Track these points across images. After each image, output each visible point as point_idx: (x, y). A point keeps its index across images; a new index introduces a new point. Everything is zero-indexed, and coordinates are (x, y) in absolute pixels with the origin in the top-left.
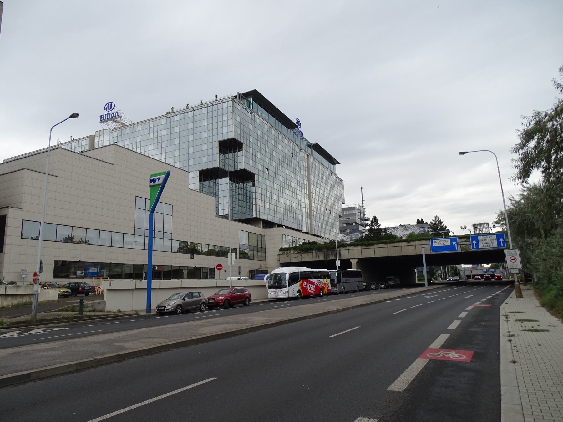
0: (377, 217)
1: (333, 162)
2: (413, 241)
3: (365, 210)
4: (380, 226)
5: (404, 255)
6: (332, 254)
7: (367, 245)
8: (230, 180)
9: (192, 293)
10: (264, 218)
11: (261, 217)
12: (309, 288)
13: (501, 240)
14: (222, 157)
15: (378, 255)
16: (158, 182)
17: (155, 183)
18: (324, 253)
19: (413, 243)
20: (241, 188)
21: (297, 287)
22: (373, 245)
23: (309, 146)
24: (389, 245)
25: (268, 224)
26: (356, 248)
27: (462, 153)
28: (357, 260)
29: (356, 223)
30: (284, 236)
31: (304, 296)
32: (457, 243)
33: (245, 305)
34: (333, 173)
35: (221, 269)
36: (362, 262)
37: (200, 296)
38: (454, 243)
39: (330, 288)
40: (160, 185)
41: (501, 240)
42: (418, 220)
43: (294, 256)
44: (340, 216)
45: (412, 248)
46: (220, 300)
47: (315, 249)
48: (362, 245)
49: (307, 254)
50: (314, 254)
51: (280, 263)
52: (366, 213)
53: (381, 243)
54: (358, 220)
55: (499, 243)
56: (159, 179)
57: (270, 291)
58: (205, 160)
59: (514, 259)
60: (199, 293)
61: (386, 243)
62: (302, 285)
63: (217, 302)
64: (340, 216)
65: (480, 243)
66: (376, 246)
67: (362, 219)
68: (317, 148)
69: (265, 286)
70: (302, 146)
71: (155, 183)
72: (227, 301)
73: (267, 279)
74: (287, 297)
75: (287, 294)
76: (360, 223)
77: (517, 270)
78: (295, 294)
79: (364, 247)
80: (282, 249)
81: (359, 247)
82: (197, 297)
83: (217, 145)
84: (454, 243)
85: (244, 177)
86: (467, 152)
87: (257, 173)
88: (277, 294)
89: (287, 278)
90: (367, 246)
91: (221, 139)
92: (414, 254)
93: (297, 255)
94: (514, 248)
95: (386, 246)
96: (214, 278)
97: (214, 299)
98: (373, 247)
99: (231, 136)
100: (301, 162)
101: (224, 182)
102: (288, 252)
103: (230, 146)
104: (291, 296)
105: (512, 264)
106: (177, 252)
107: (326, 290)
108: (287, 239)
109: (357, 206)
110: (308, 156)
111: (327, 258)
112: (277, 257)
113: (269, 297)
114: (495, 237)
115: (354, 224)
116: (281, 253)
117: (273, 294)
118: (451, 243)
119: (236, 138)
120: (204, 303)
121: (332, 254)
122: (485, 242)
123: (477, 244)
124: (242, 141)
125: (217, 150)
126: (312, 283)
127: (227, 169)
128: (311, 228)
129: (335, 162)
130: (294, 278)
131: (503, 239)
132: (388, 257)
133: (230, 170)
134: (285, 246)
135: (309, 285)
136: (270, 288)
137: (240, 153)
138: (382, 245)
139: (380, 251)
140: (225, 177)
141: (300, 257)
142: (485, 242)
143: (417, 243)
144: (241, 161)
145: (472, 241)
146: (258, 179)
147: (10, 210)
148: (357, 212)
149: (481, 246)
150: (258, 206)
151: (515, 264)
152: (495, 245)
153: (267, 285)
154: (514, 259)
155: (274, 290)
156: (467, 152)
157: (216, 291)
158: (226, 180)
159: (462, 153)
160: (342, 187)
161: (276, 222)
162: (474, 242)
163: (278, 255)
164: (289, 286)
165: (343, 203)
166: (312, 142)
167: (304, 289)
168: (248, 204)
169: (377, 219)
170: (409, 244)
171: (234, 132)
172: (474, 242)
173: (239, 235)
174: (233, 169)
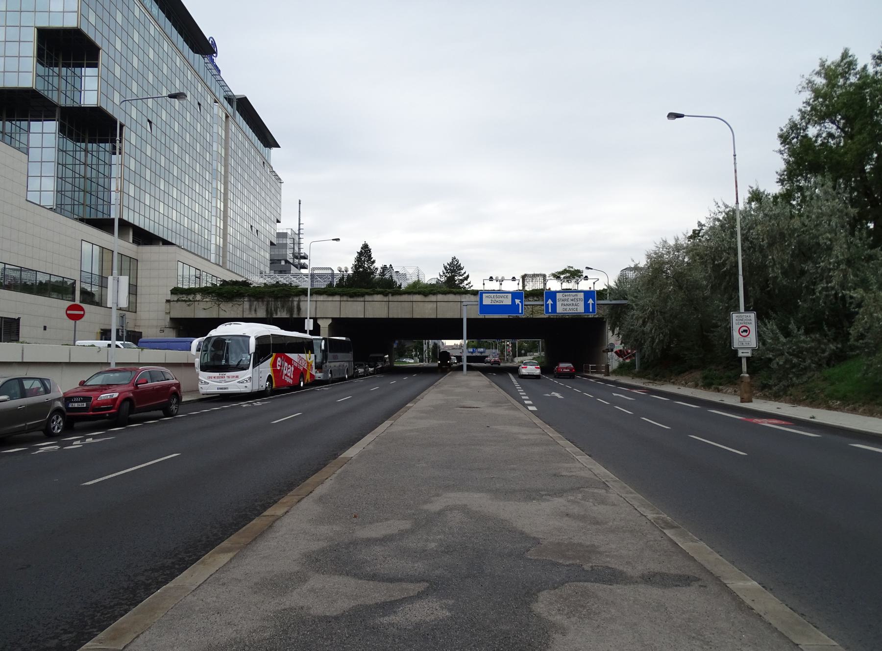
0: (370, 246)
1: (268, 141)
2: (434, 294)
3: (302, 241)
4: (374, 262)
5: (416, 316)
6: (283, 307)
7: (352, 295)
8: (62, 129)
9: (20, 380)
10: (136, 224)
11: (131, 221)
12: (285, 372)
13: (591, 301)
14: (42, 70)
15: (370, 315)
18: (267, 305)
19: (432, 298)
20: (86, 151)
21: (266, 368)
22: (363, 295)
23: (230, 99)
24: (391, 298)
25: (144, 237)
26: (330, 298)
27: (673, 116)
28: (330, 321)
29: (287, 261)
30: (180, 264)
31: (277, 389)
32: (521, 302)
33: (168, 413)
34: (265, 163)
35: (79, 317)
36: (338, 325)
37: (47, 391)
38: (517, 301)
39: (313, 373)
43: (202, 305)
44: (272, 244)
45: (430, 305)
46: (105, 402)
47: (249, 296)
48: (342, 295)
49: (231, 305)
50: (246, 305)
51: (173, 320)
52: (302, 246)
53: (378, 293)
54: (290, 257)
55: (586, 306)
57: (204, 376)
59: (745, 331)
60: (42, 380)
61: (386, 295)
62: (274, 365)
63: (98, 407)
64: (272, 244)
65: (559, 304)
66: (367, 298)
67: (295, 257)
68: (244, 107)
69: (192, 365)
70: (217, 94)
72: (128, 404)
73: (198, 350)
74: (248, 390)
75: (249, 384)
76: (291, 261)
77: (749, 351)
78: (264, 384)
79: (345, 298)
80: (175, 291)
81: (337, 298)
82: (35, 392)
83: (31, 36)
84: (517, 301)
85: (92, 127)
86: (681, 116)
87: (128, 124)
88: (223, 385)
89: (252, 349)
90: (351, 296)
91: (44, 24)
92: (434, 316)
93: (209, 305)
94: (747, 309)
95: (386, 299)
96: (17, 340)
97: (86, 399)
98: (362, 299)
99: (71, 22)
100: (215, 126)
101: (44, 134)
102: (191, 297)
103: (65, 48)
104: (256, 388)
105: (742, 339)
106: (54, 210)
107: (308, 377)
108: (186, 273)
109: (289, 232)
110: (227, 117)
111: (272, 314)
112: (164, 306)
113: (202, 391)
114: (582, 295)
115: (283, 263)
116: (175, 298)
117: (212, 383)
119: (85, 29)
120: (58, 411)
121: (283, 307)
122: (566, 303)
123: (554, 306)
124: (98, 42)
125: (30, 48)
126: (290, 361)
127: (55, 99)
128: (224, 257)
129: (271, 141)
130: (265, 348)
131: (594, 300)
132: (437, 319)
133: (62, 103)
134: (180, 286)
135: (286, 364)
136: (205, 368)
137: (89, 71)
139: (375, 308)
140: (49, 117)
141: (216, 308)
142: (566, 303)
143: (440, 297)
144: (90, 87)
145: (547, 301)
146: (130, 138)
148: (289, 241)
149: (560, 309)
150: (126, 196)
151: (747, 339)
152: (581, 309)
153: (197, 361)
154: (745, 331)
155: (217, 374)
156: (681, 116)
157: (84, 374)
158: (52, 126)
159: (673, 116)
160: (279, 191)
161: (161, 236)
163: (168, 301)
164: (254, 367)
165: (278, 221)
166: (237, 92)
167: (277, 372)
168: (100, 188)
169: (370, 250)
170: (427, 299)
171: (81, 15)
172: (550, 302)
173: (75, 251)
174: (69, 103)
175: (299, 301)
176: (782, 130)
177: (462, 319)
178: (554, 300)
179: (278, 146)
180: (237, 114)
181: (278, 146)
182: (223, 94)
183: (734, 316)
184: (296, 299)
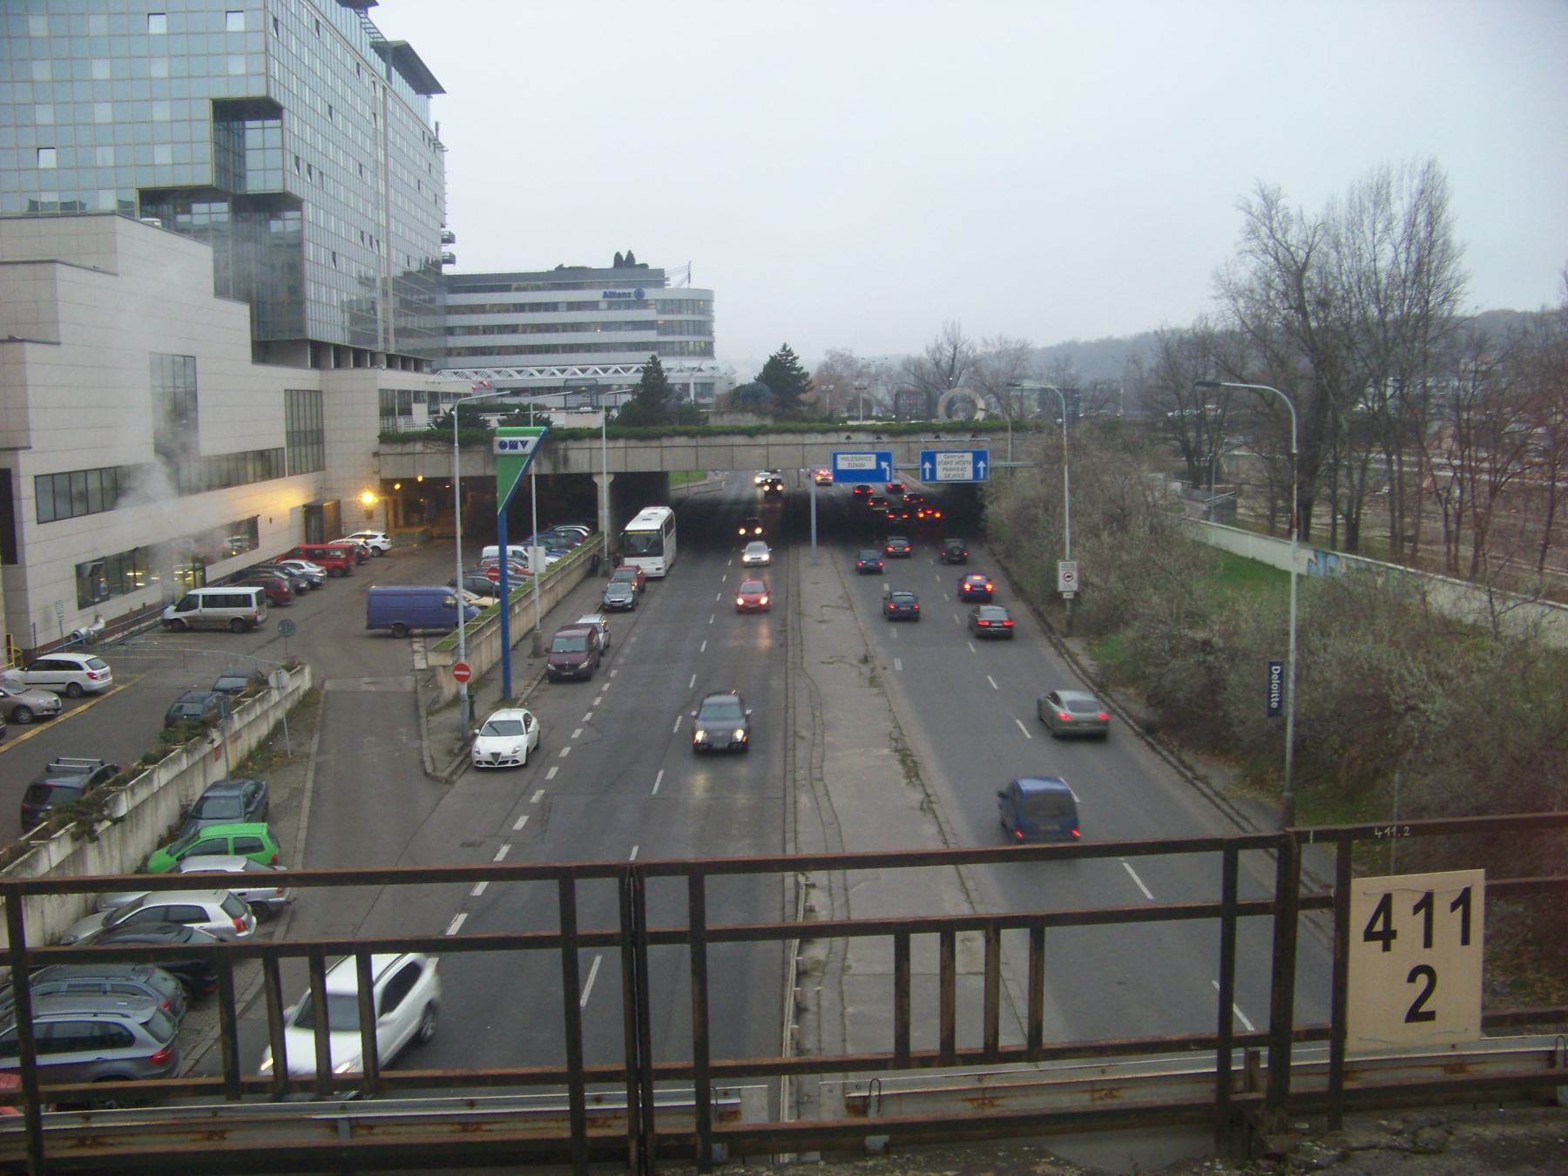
1: (425, 83)
16: (520, 450)
17: (513, 452)
19: (761, 440)
22: (658, 437)
24: (701, 441)
38: (884, 465)
40: (523, 456)
41: (981, 465)
42: (618, 256)
48: (628, 437)
55: (976, 471)
56: (524, 444)
58: (163, 155)
65: (939, 468)
66: (666, 442)
71: (513, 452)
79: (633, 443)
83: (206, 111)
84: (884, 465)
91: (223, 93)
94: (1072, 559)
95: (693, 442)
116: (386, 449)
118: (878, 465)
123: (933, 471)
138: (682, 441)
143: (773, 439)
147: (22, 455)
149: (941, 475)
162: (927, 466)
163: (376, 454)
166: (392, 35)
175: (566, 449)
176: (1137, 363)
177: (819, 542)
178: (933, 463)
179: (442, 91)
180: (395, 74)
181: (442, 91)
182: (367, 40)
183: (1061, 564)
184: (562, 446)
